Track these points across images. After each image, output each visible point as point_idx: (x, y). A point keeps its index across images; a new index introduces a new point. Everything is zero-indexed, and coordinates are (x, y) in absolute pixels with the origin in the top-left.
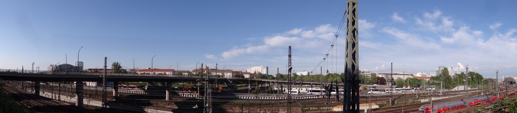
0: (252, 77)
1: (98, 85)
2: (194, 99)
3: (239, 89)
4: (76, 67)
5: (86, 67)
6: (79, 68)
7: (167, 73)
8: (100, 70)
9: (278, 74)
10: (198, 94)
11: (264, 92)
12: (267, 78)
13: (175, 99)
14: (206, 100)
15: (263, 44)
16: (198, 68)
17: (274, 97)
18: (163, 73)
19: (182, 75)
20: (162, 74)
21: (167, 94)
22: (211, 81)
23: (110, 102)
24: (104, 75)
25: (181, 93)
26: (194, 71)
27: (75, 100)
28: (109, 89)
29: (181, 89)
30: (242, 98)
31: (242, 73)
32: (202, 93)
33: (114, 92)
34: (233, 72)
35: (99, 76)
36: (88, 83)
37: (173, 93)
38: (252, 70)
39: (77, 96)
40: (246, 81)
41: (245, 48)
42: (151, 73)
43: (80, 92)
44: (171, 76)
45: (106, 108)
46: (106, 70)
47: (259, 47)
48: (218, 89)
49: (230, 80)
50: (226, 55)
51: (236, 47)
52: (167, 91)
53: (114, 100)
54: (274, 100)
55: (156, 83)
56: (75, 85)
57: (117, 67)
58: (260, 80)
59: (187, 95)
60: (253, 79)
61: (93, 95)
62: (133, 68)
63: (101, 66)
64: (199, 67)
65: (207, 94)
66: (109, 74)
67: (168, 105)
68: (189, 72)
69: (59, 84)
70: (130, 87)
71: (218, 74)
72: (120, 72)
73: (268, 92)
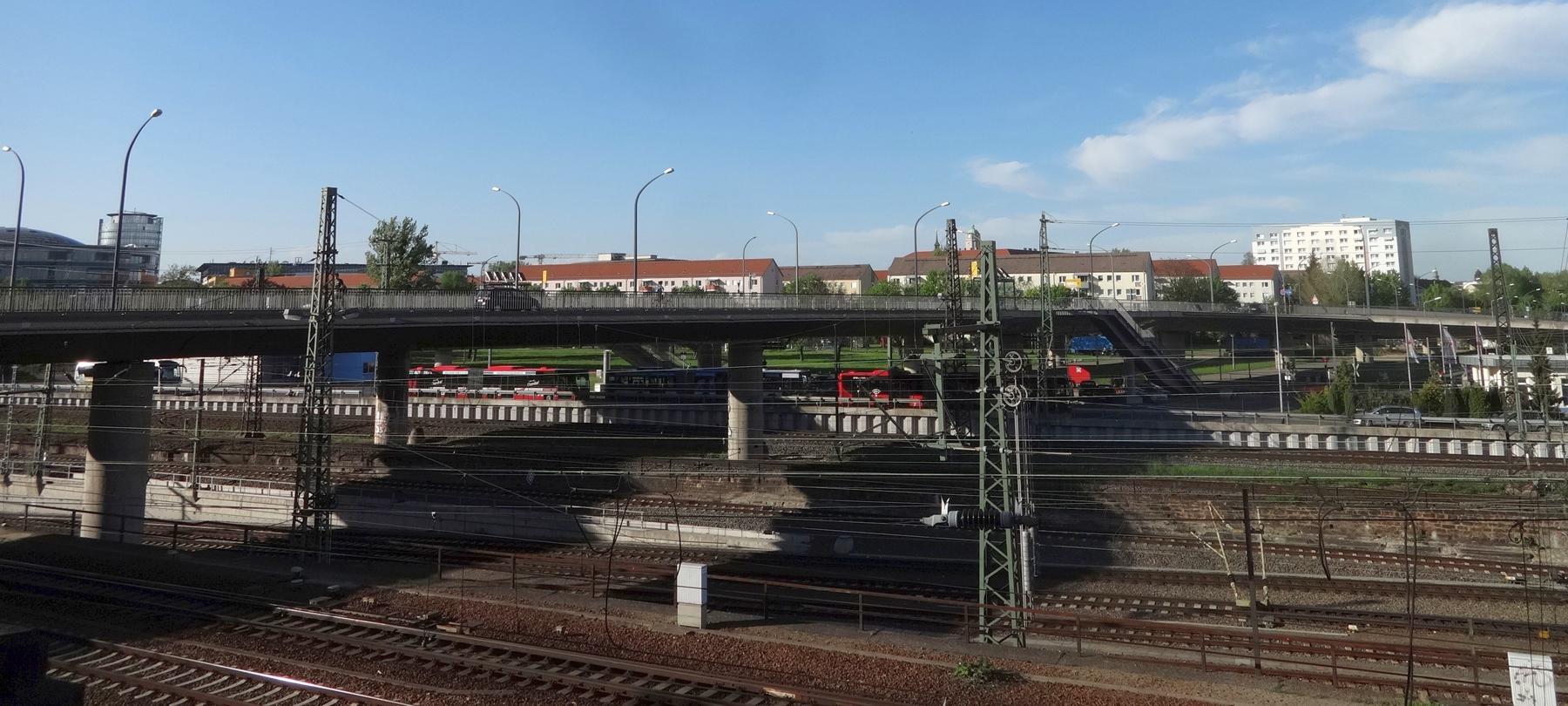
0: (1294, 300)
1: (270, 375)
2: (903, 452)
3: (1209, 376)
4: (101, 253)
5: (180, 252)
6: (126, 257)
7: (731, 284)
8: (287, 269)
9: (1499, 271)
10: (939, 413)
12: (1405, 304)
13: (780, 444)
14: (993, 453)
15: (1348, 65)
16: (926, 246)
17: (1481, 440)
18: (704, 282)
19: (824, 292)
20: (698, 292)
21: (732, 415)
22: (1017, 330)
23: (352, 489)
24: (312, 303)
25: (821, 410)
26: (899, 265)
27: (75, 493)
28: (347, 401)
29: (824, 383)
30: (1235, 439)
31: (1220, 272)
32: (961, 412)
33: (380, 418)
34: (1155, 269)
35: (277, 313)
36: (190, 369)
37: (775, 414)
38: (1291, 249)
39: (91, 464)
40: (1252, 332)
41: (1229, 105)
42: (626, 286)
43: (121, 435)
44: (758, 303)
45: (320, 535)
46: (329, 269)
47: (1324, 95)
48: (1058, 379)
49: (1140, 317)
50: (1101, 155)
51: (1163, 104)
52: (732, 401)
53: (380, 471)
54: (1486, 459)
55: (662, 351)
56: (84, 383)
57: (404, 251)
58: (1353, 313)
59: (859, 420)
60: (1301, 312)
61: (225, 448)
62: (510, 258)
63: (296, 244)
64: (931, 237)
65: (993, 419)
66: (352, 302)
67: (746, 486)
68: (867, 275)
70: (490, 381)
71: (1054, 279)
72: (426, 285)
73: (1432, 405)
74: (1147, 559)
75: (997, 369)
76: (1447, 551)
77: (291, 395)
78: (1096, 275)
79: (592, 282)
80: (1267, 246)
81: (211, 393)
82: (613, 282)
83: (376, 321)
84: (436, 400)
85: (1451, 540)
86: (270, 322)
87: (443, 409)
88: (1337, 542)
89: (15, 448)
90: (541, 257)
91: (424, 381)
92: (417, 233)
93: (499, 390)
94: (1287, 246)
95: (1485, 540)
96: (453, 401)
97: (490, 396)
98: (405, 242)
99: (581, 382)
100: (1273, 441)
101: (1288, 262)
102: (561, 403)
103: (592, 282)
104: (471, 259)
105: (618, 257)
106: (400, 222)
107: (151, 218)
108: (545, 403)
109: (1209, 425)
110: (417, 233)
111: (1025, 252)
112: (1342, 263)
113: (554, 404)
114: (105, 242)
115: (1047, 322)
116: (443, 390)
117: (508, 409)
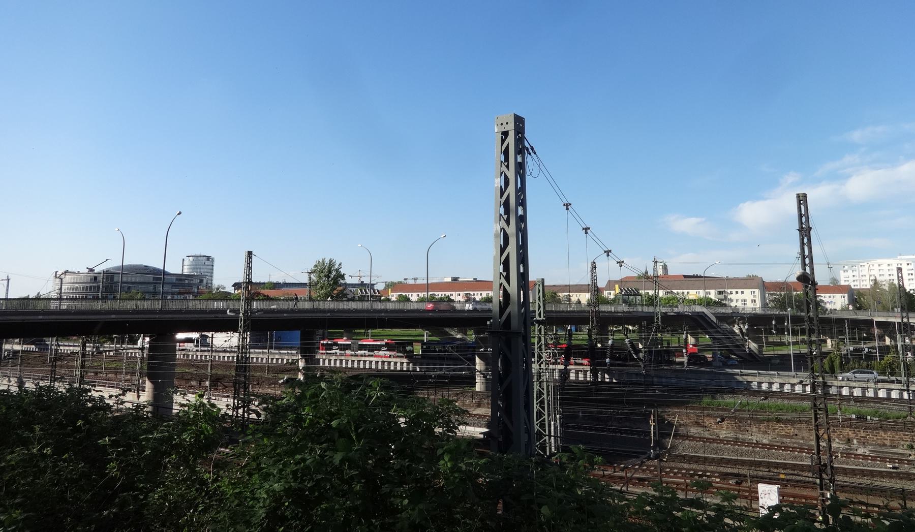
4: (181, 278)
7: (574, 297)
11: (869, 369)
34: (765, 287)
35: (224, 312)
39: (148, 385)
57: (329, 278)
69: (84, 346)
74: (685, 448)
75: (543, 342)
76: (861, 451)
77: (263, 353)
78: (729, 291)
79: (436, 293)
80: (850, 273)
81: (216, 351)
82: (448, 294)
83: (190, 316)
84: (334, 357)
85: (864, 444)
86: (220, 315)
87: (338, 362)
88: (798, 443)
89: (129, 377)
90: (416, 279)
91: (328, 347)
92: (336, 267)
93: (367, 353)
94: (863, 273)
95: (884, 445)
96: (343, 358)
97: (362, 356)
98: (330, 272)
99: (409, 348)
100: (787, 388)
101: (864, 283)
102: (398, 360)
103: (436, 293)
104: (377, 280)
105: (455, 279)
106: (327, 261)
107: (208, 258)
108: (390, 360)
109: (750, 379)
110: (336, 267)
111: (693, 277)
112: (891, 284)
113: (395, 360)
114: (186, 272)
115: (658, 319)
116: (338, 351)
117: (371, 362)
